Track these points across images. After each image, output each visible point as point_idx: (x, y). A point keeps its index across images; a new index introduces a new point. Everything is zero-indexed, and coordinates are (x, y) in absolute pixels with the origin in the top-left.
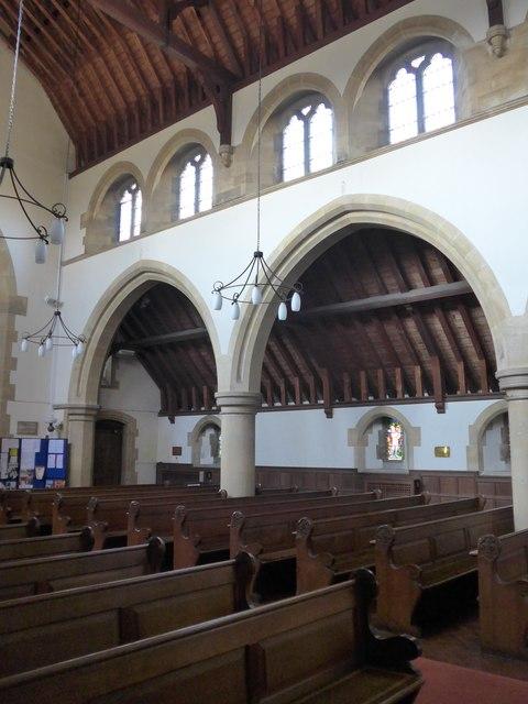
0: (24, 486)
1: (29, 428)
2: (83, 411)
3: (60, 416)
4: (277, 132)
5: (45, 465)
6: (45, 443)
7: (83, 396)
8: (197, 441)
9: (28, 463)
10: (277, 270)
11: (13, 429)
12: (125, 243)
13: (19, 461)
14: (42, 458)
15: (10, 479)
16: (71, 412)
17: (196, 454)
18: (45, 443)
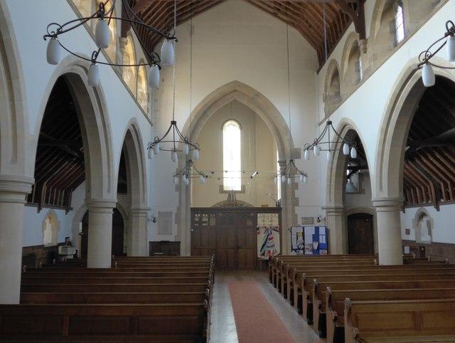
0: (308, 252)
1: (308, 221)
2: (334, 210)
3: (323, 214)
4: (391, 19)
5: (318, 240)
6: (317, 229)
7: (333, 201)
8: (418, 225)
9: (309, 240)
10: (341, 133)
11: (300, 222)
12: (45, 218)
13: (304, 239)
14: (316, 237)
15: (299, 249)
16: (329, 210)
17: (418, 234)
18: (317, 229)
